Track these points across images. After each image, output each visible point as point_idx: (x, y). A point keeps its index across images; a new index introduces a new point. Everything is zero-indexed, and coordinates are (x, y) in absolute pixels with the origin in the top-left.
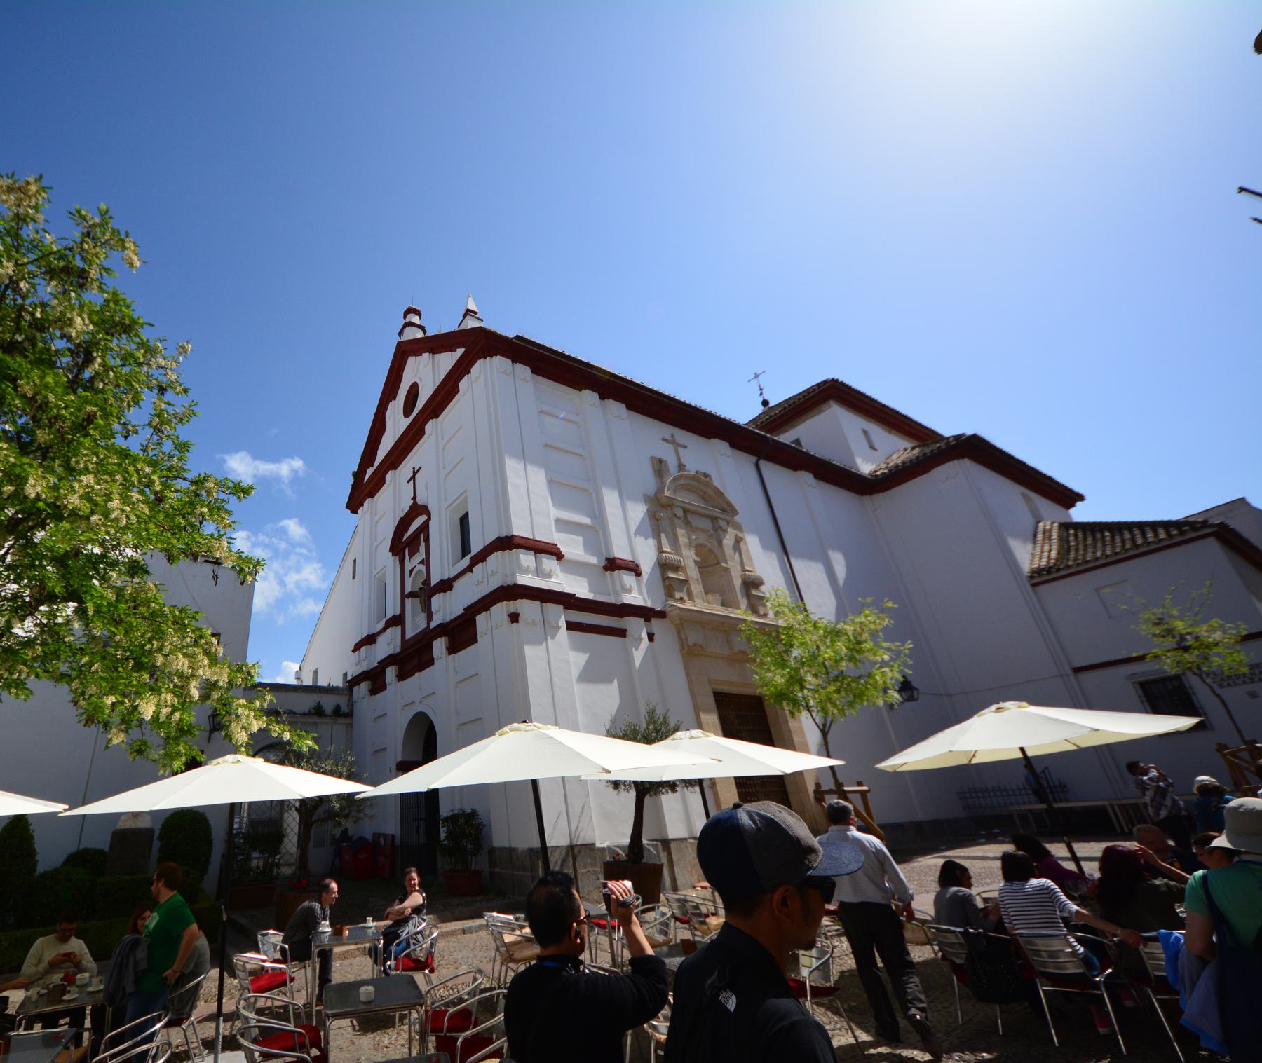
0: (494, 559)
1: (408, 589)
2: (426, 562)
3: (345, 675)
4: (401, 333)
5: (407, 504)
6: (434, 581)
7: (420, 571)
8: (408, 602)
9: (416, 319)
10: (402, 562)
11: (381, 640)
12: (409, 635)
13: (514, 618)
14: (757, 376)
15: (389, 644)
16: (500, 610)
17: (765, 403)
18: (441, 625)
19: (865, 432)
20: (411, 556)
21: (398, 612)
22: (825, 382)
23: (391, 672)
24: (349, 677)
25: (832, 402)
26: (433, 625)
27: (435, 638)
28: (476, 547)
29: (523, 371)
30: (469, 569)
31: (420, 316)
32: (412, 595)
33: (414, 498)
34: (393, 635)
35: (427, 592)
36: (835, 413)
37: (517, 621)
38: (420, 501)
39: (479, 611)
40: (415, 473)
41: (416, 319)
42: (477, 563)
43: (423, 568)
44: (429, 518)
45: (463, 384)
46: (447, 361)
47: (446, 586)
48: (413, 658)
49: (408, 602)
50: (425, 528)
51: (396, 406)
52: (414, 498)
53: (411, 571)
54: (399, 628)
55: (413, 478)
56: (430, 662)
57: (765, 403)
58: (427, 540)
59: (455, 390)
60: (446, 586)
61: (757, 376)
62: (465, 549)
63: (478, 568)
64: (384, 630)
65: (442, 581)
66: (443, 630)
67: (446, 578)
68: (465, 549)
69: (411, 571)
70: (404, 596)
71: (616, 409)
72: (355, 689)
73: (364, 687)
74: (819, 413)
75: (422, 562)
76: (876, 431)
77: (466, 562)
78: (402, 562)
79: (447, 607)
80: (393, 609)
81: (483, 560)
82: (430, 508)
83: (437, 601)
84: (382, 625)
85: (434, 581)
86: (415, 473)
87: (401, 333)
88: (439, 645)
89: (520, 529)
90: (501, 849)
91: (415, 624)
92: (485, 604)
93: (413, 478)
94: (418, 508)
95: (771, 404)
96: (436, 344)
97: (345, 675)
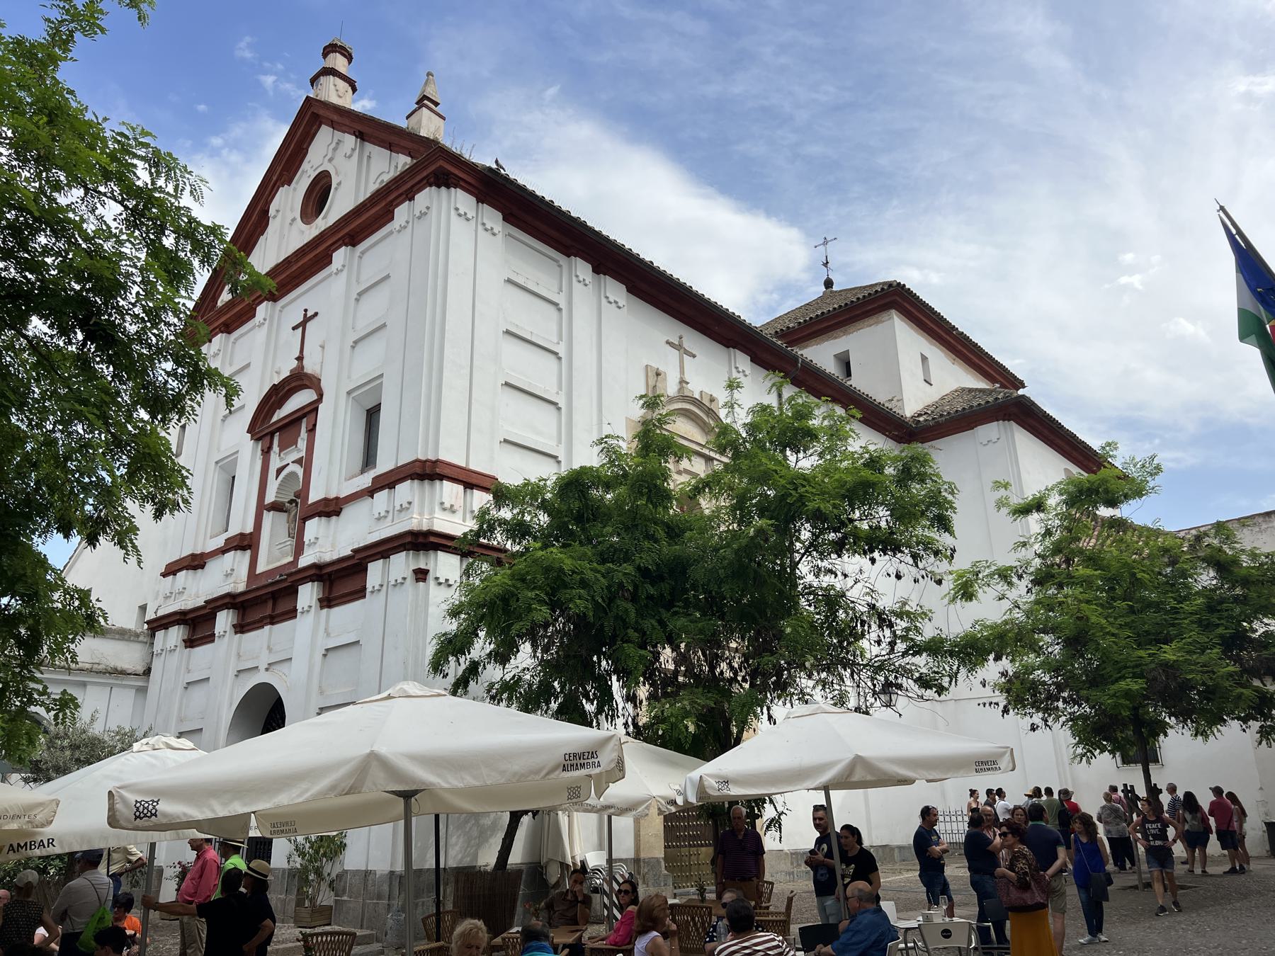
0: (405, 490)
1: (270, 497)
2: (306, 463)
3: (143, 608)
4: (314, 81)
5: (286, 367)
6: (314, 497)
7: (293, 475)
8: (268, 517)
9: (338, 62)
10: (266, 452)
11: (216, 568)
12: (261, 568)
13: (421, 575)
14: (826, 242)
15: (229, 575)
16: (402, 564)
17: (828, 284)
18: (314, 566)
19: (924, 359)
20: (282, 448)
21: (249, 529)
22: (890, 285)
23: (224, 620)
24: (150, 615)
25: (893, 312)
26: (304, 562)
27: (304, 581)
28: (385, 464)
29: (492, 217)
30: (370, 492)
31: (350, 58)
32: (276, 507)
33: (300, 358)
34: (238, 562)
35: (302, 509)
36: (899, 329)
37: (424, 580)
38: (310, 367)
39: (374, 558)
40: (307, 320)
41: (338, 62)
42: (381, 488)
43: (300, 471)
44: (320, 399)
45: (402, 212)
46: (386, 166)
47: (331, 508)
48: (264, 603)
49: (268, 517)
50: (311, 410)
51: (289, 200)
52: (300, 358)
53: (279, 471)
54: (248, 552)
55: (303, 324)
56: (292, 614)
57: (828, 284)
58: (312, 430)
59: (387, 216)
60: (331, 508)
61: (826, 242)
62: (369, 459)
63: (382, 496)
64: (223, 551)
65: (326, 501)
66: (318, 573)
67: (332, 496)
68: (369, 459)
69: (279, 471)
70: (262, 507)
71: (615, 290)
72: (160, 635)
73: (175, 635)
74: (877, 323)
75: (298, 461)
76: (939, 358)
77: (366, 481)
78: (266, 452)
79: (329, 541)
80: (242, 522)
81: (391, 486)
82: (323, 384)
83: (313, 527)
84: (219, 542)
85: (314, 497)
86: (307, 320)
87: (314, 81)
88: (308, 594)
89: (451, 453)
90: (356, 873)
91: (273, 554)
92: (384, 549)
93: (303, 324)
94: (299, 380)
95: (835, 288)
96: (369, 131)
97: (143, 608)
